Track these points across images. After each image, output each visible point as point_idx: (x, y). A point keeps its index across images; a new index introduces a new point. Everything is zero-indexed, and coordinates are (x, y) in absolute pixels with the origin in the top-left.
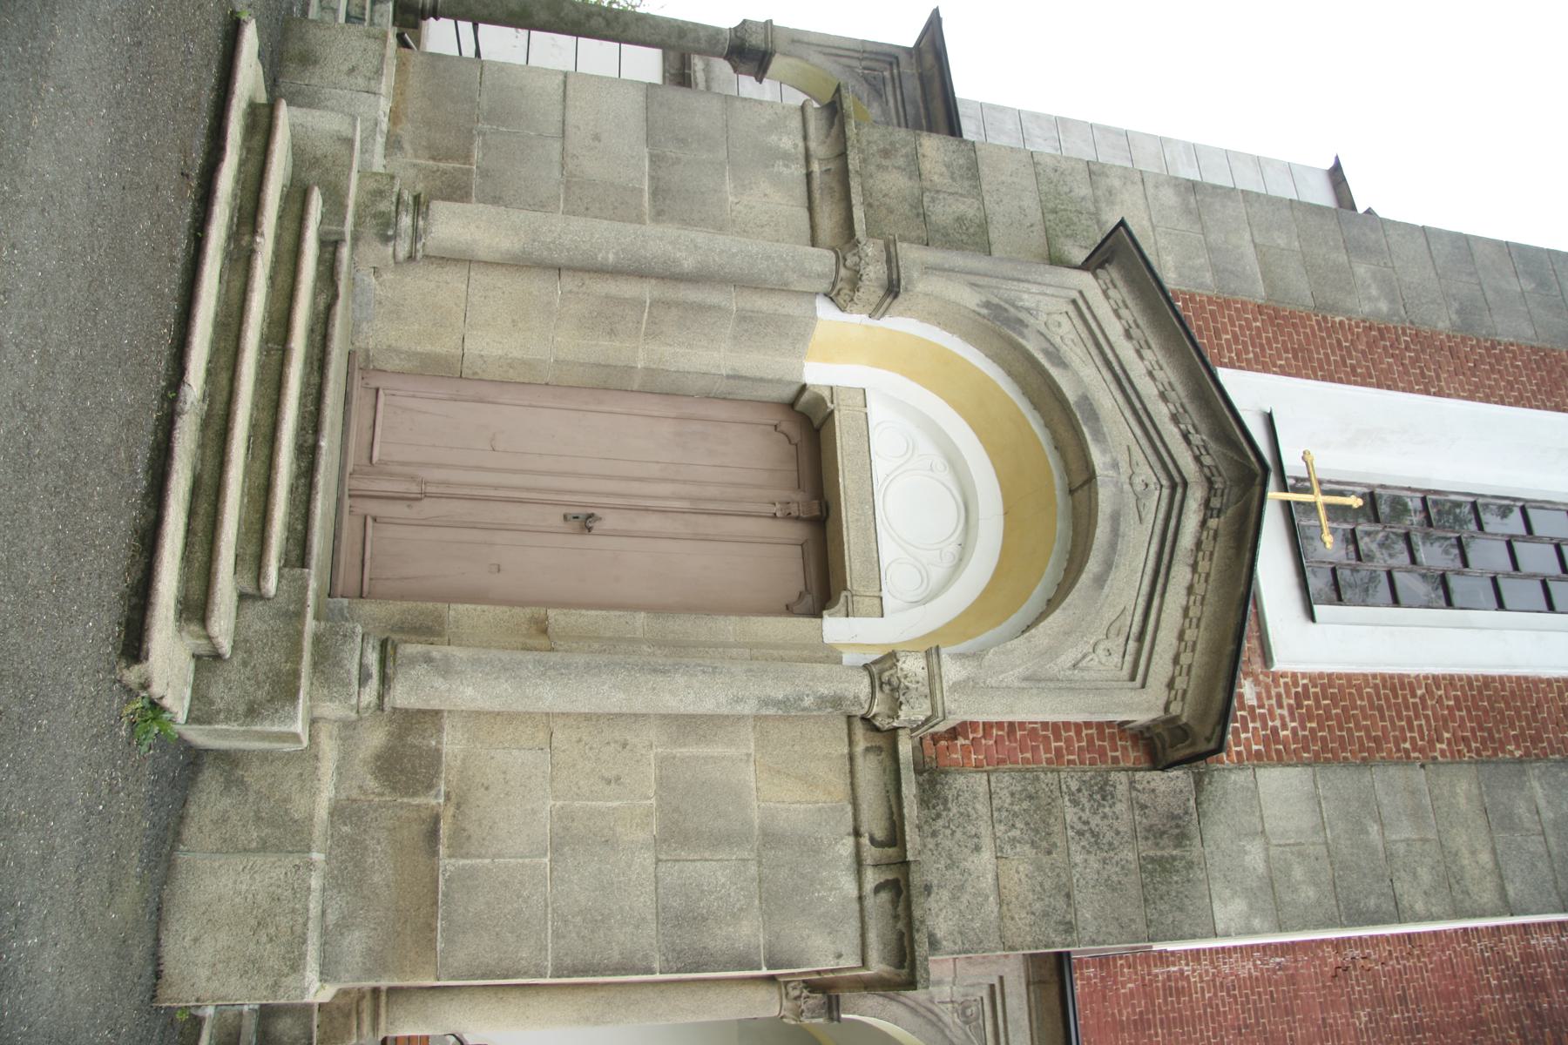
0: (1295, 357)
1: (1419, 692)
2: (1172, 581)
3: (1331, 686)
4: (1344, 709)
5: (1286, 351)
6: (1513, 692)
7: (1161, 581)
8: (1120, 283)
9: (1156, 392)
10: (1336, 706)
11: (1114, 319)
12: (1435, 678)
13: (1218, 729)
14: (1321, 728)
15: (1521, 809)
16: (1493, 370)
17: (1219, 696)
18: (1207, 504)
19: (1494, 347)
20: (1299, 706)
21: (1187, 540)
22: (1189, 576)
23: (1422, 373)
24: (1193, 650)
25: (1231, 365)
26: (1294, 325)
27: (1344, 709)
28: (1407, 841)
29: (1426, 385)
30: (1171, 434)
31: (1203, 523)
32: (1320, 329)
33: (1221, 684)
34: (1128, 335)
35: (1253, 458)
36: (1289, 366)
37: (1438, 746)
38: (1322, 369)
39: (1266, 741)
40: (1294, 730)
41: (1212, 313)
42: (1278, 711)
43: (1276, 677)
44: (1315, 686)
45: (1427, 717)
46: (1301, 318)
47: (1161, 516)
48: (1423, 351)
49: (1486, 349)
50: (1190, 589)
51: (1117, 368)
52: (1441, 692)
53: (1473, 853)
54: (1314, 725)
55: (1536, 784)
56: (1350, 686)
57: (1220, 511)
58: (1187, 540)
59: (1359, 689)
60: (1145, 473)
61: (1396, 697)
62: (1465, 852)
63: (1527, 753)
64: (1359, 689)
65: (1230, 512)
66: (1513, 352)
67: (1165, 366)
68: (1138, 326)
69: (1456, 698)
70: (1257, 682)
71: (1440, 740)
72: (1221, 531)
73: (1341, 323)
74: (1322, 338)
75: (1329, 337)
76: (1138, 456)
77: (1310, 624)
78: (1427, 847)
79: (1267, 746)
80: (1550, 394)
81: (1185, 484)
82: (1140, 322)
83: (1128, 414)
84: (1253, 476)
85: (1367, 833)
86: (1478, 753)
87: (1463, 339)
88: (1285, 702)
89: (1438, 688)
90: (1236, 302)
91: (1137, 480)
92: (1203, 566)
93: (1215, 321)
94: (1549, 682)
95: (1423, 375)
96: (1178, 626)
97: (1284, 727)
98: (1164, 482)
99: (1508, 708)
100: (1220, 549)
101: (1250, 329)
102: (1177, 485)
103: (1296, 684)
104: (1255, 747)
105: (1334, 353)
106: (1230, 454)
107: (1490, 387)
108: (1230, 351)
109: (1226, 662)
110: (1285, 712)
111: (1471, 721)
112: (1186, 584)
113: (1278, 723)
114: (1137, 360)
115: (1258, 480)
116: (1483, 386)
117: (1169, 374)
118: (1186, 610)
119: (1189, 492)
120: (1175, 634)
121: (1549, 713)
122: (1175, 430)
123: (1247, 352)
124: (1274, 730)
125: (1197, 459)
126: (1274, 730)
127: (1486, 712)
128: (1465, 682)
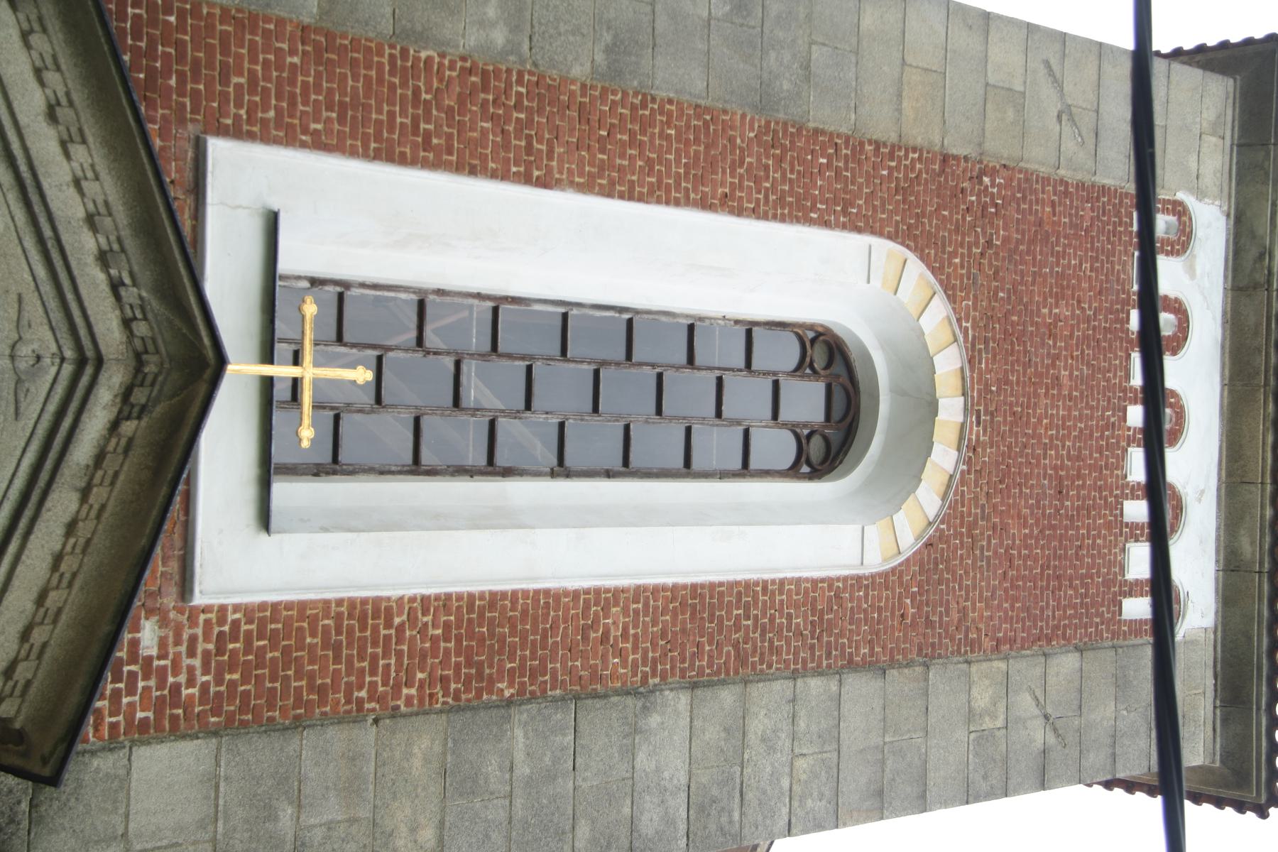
0: (342, 119)
1: (397, 620)
2: (45, 515)
3: (274, 620)
4: (286, 651)
5: (330, 108)
6: (525, 612)
7: (28, 513)
8: (53, 24)
9: (81, 213)
10: (273, 647)
11: (33, 84)
12: (425, 600)
13: (61, 748)
14: (245, 680)
15: (492, 767)
16: (632, 142)
17: (75, 699)
18: (126, 395)
19: (644, 105)
20: (220, 650)
21: (82, 452)
22: (74, 506)
23: (529, 146)
24: (55, 622)
25: (236, 133)
26: (354, 63)
27: (286, 651)
28: (330, 826)
29: (529, 165)
30: (93, 280)
31: (114, 426)
32: (392, 73)
33: (81, 682)
34: (52, 115)
35: (206, 341)
36: (328, 131)
37: (405, 691)
38: (378, 138)
39: (159, 706)
40: (205, 688)
41: (224, 37)
42: (186, 662)
43: (194, 614)
44: (250, 622)
45: (399, 654)
46: (368, 50)
47: (52, 407)
48: (540, 111)
49: (634, 108)
50: (71, 528)
51: (23, 168)
52: (428, 619)
53: (413, 830)
54: (236, 676)
55: (519, 733)
56: (302, 617)
57: (143, 408)
58: (82, 452)
59: (314, 621)
60: (41, 339)
61: (363, 628)
62: (403, 829)
63: (521, 692)
64: (314, 621)
65: (159, 410)
66: (670, 114)
67: (104, 175)
68: (71, 104)
69: (447, 626)
70: (164, 622)
71: (409, 684)
72: (138, 441)
73: (429, 60)
74: (392, 87)
75: (404, 84)
76: (34, 310)
77: (264, 536)
78: (354, 829)
79: (159, 713)
80: (700, 180)
81: (100, 362)
82: (76, 97)
83: (30, 242)
84: (202, 363)
85: (276, 819)
86: (457, 697)
87: (605, 91)
88: (201, 647)
89: (425, 613)
90: (267, 20)
91: (25, 350)
92: (98, 496)
93: (225, 51)
94: (576, 594)
95: (529, 149)
96: (41, 583)
97: (191, 682)
98: (69, 354)
99: (513, 632)
100: (129, 470)
101: (280, 68)
102: (88, 361)
103: (222, 620)
104: (140, 715)
105: (403, 112)
106: (178, 323)
107: (621, 169)
108: (239, 105)
109: (95, 649)
110: (197, 662)
111: (458, 654)
112: (67, 518)
113: (182, 678)
114: (60, 158)
115: (208, 374)
116: (612, 167)
117: (108, 188)
118: (58, 559)
119: (103, 377)
120: (34, 595)
121: (565, 635)
122: (101, 276)
123: (266, 109)
124: (176, 688)
125: (127, 323)
126: (176, 688)
127: (482, 640)
128: (464, 604)
